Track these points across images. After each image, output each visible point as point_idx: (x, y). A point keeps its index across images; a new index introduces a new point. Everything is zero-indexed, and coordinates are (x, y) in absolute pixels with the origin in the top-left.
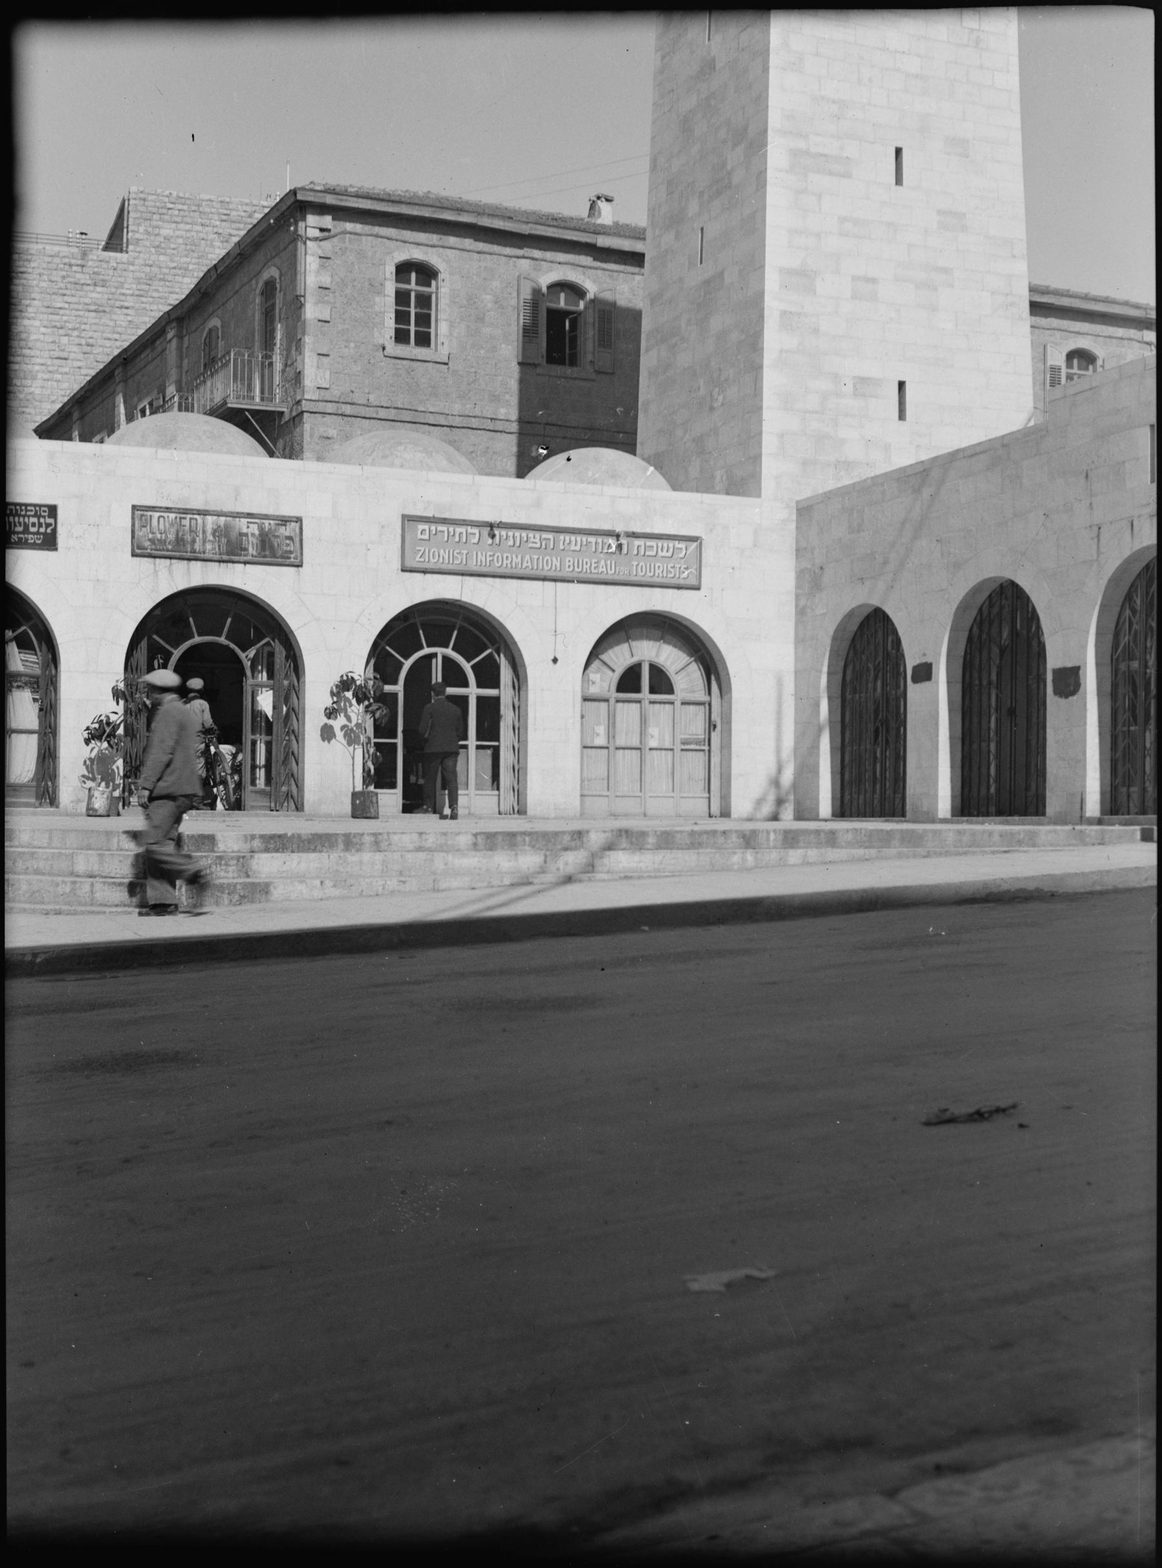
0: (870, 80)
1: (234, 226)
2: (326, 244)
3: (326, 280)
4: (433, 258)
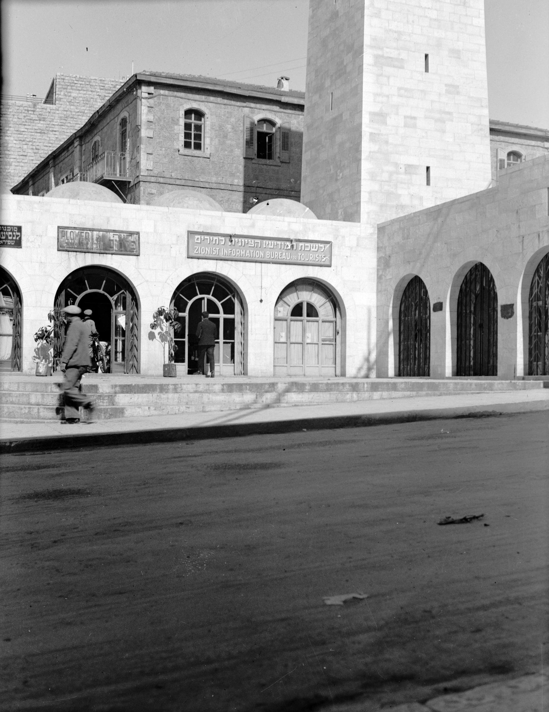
0: (413, 22)
1: (107, 92)
2: (151, 101)
3: (151, 118)
4: (202, 107)
